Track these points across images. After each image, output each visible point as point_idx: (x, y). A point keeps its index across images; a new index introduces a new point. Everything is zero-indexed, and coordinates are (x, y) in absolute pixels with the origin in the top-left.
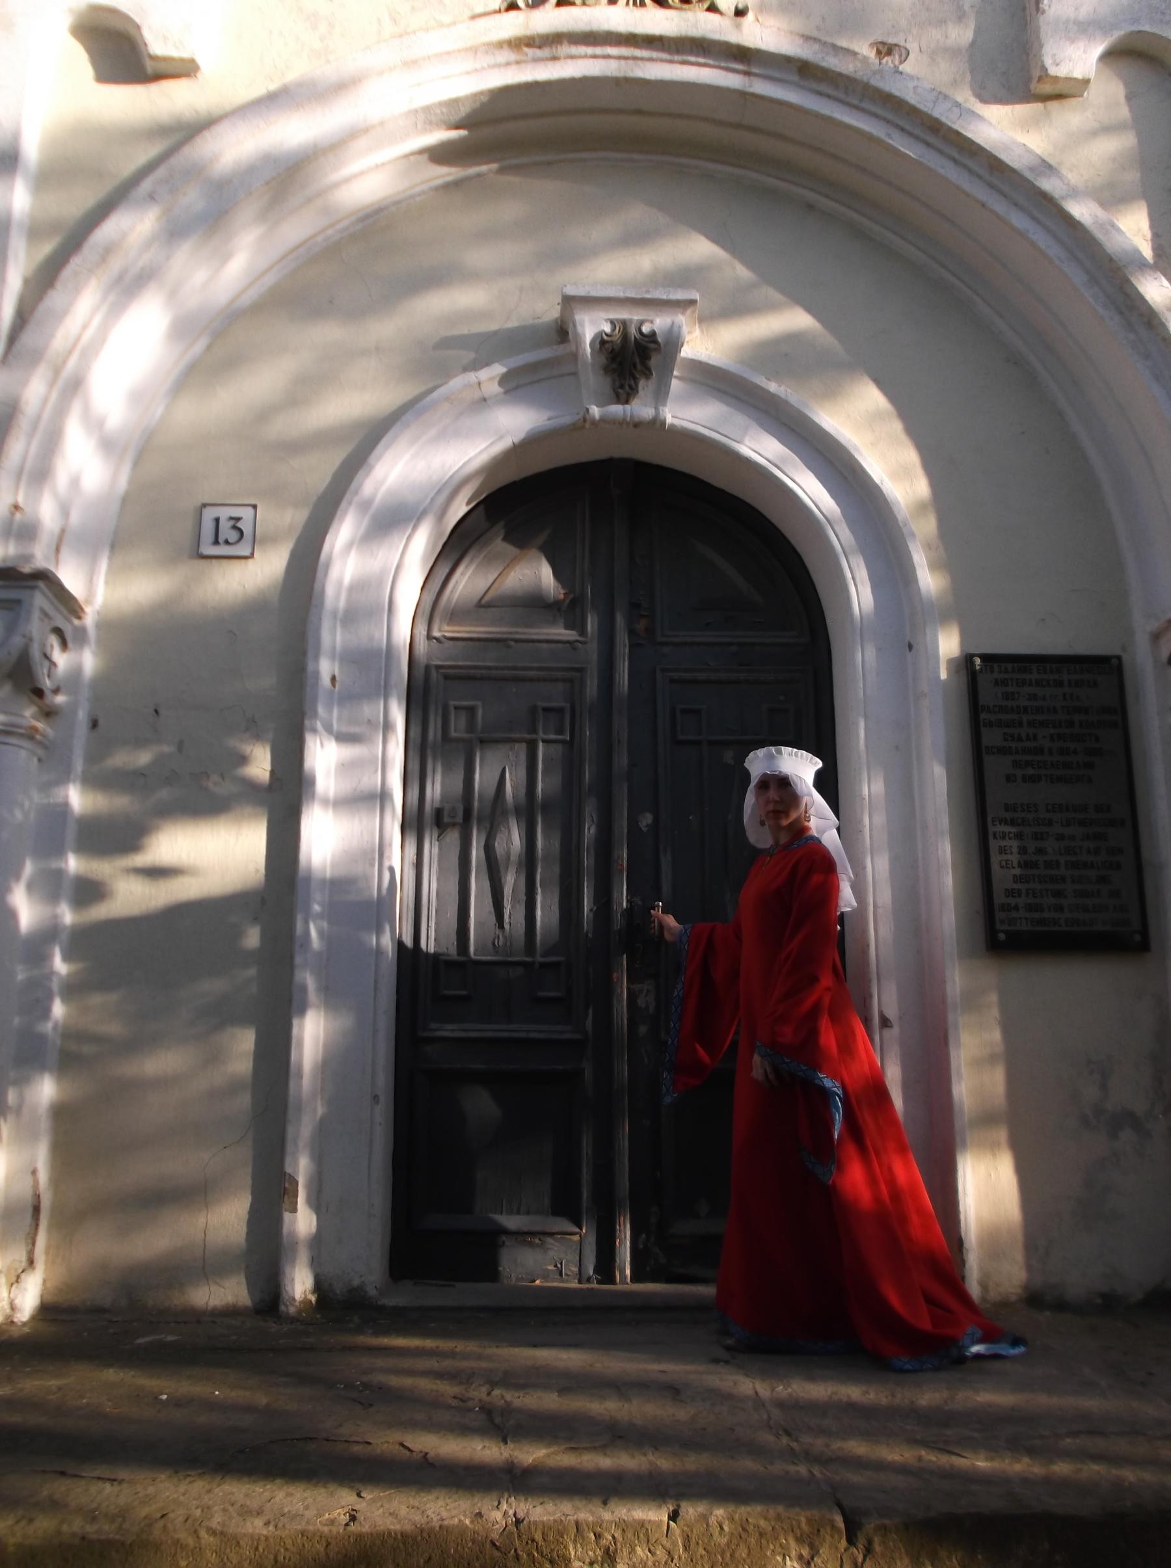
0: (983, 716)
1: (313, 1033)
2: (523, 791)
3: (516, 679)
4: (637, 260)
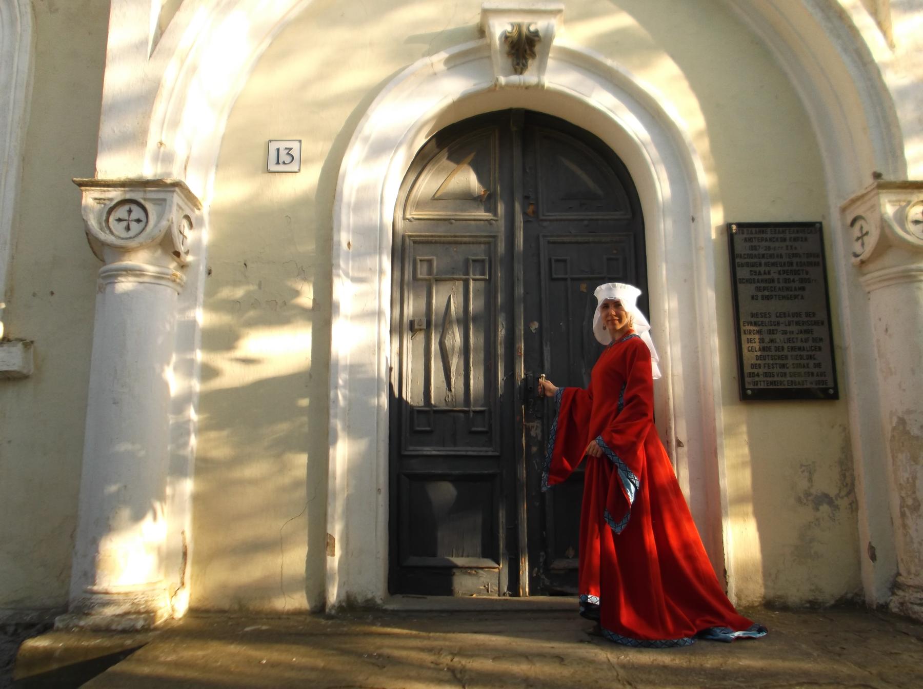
0: (737, 260)
1: (342, 453)
2: (462, 309)
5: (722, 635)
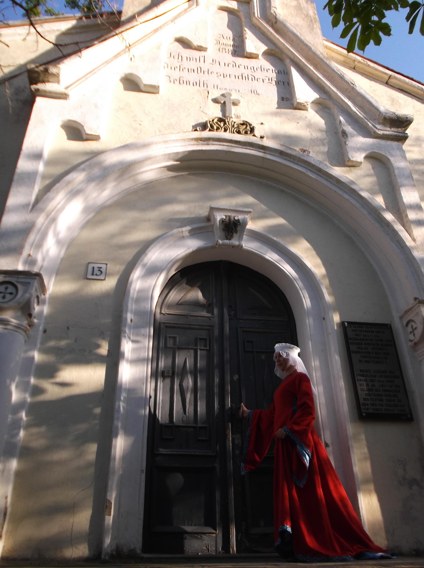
0: (350, 341)
1: (120, 444)
2: (193, 366)
3: (190, 329)
4: (231, 201)
5: (371, 555)
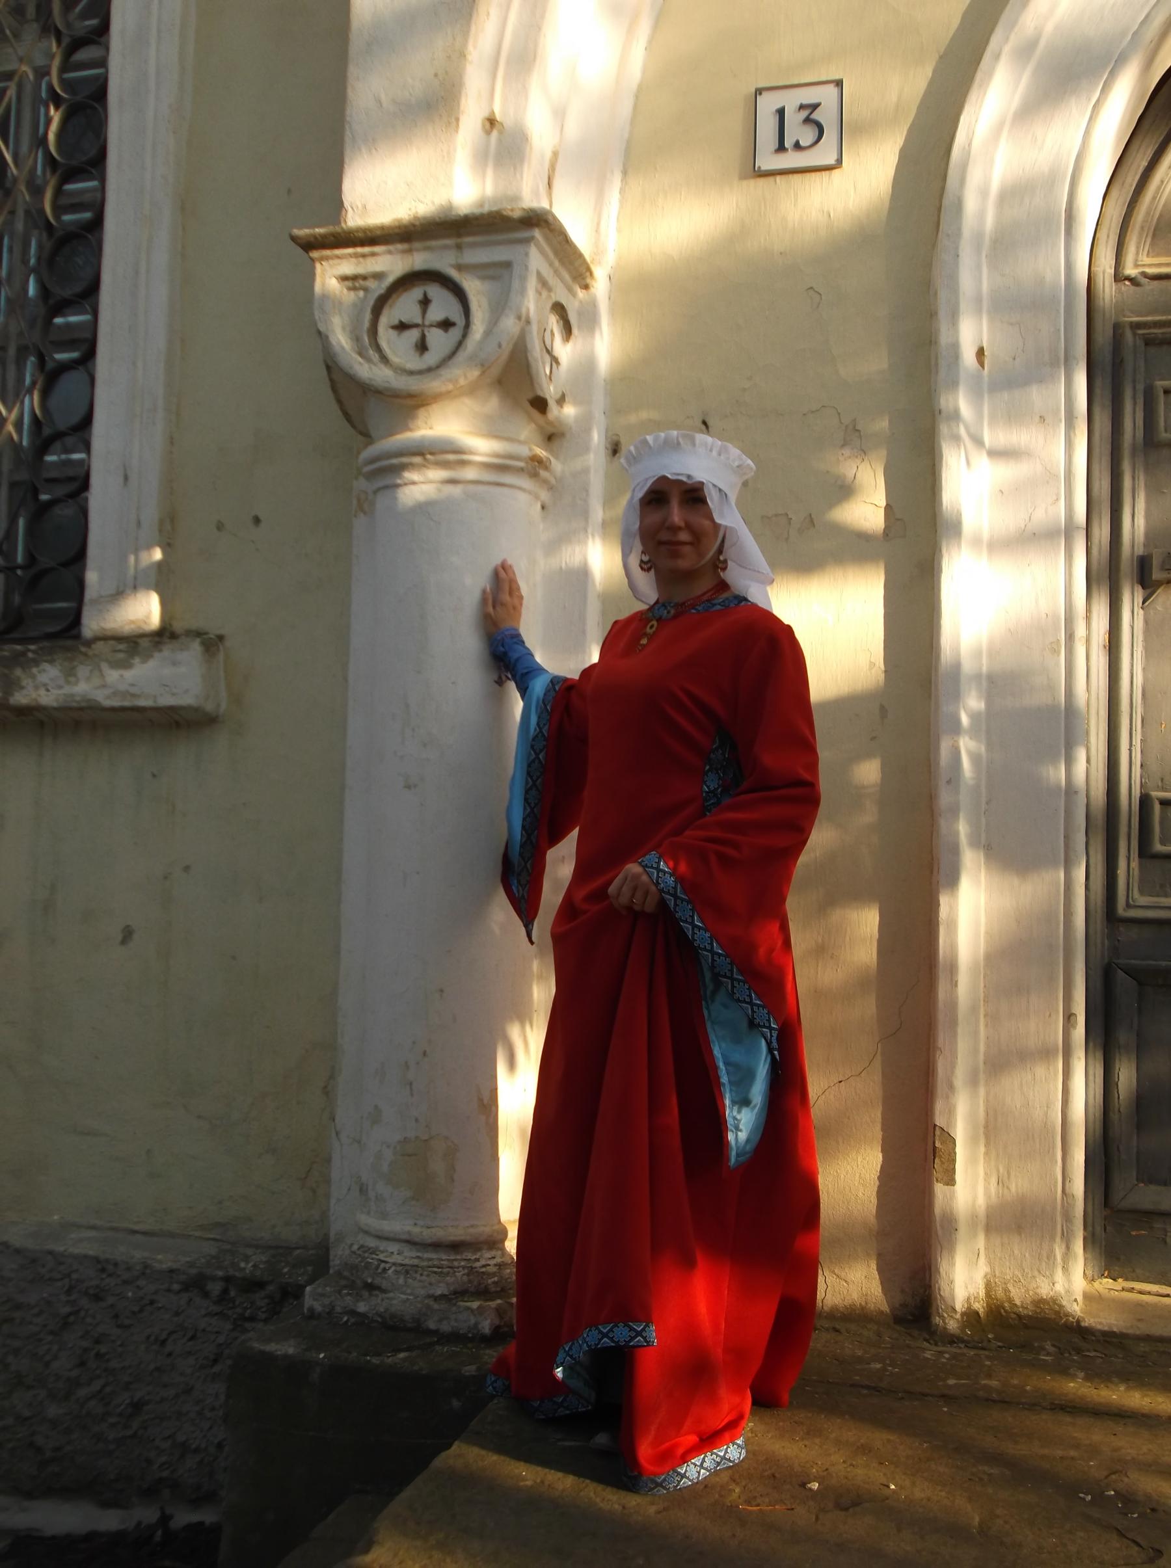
1: (974, 910)
